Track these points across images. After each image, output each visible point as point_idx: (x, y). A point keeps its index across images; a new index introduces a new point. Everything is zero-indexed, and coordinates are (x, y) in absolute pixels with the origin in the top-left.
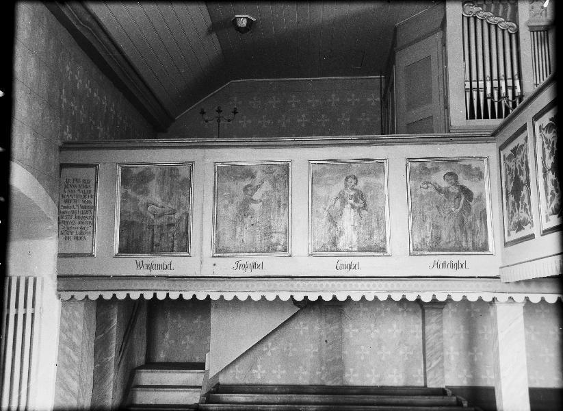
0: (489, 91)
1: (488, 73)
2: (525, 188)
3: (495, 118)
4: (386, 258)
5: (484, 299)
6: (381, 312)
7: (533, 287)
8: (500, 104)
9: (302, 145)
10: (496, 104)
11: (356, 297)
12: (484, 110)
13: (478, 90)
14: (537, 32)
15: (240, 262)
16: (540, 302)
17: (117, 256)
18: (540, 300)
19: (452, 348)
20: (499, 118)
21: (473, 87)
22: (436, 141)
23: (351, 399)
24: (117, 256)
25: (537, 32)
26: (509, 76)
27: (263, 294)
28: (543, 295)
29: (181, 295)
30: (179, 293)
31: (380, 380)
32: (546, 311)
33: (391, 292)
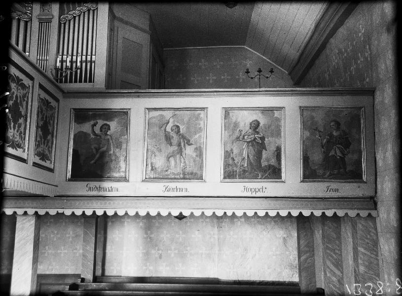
0: (79, 64)
1: (80, 51)
2: (50, 135)
3: (62, 83)
4: (203, 184)
5: (140, 214)
6: (62, 222)
7: (272, 203)
8: (76, 72)
9: (297, 94)
10: (74, 73)
11: (164, 213)
12: (70, 76)
13: (86, 61)
14: (46, 23)
15: (330, 188)
16: (368, 216)
17: (69, 180)
18: (146, 214)
19: (386, 254)
20: (64, 83)
21: (73, 60)
22: (281, 94)
23: (146, 287)
24: (69, 180)
25: (46, 23)
26: (84, 53)
27: (192, 210)
28: (192, 210)
29: (84, 212)
30: (288, 211)
31: (91, 270)
32: (143, 221)
33: (216, 209)
